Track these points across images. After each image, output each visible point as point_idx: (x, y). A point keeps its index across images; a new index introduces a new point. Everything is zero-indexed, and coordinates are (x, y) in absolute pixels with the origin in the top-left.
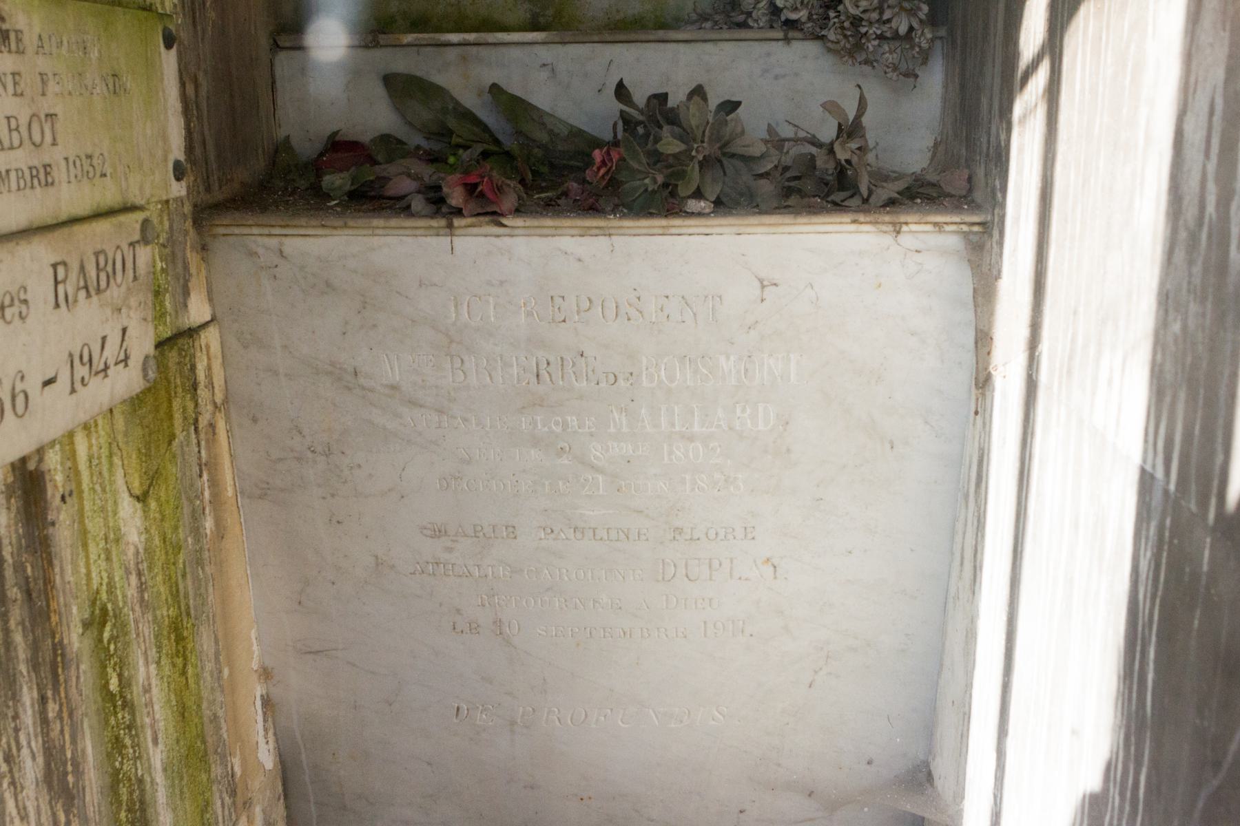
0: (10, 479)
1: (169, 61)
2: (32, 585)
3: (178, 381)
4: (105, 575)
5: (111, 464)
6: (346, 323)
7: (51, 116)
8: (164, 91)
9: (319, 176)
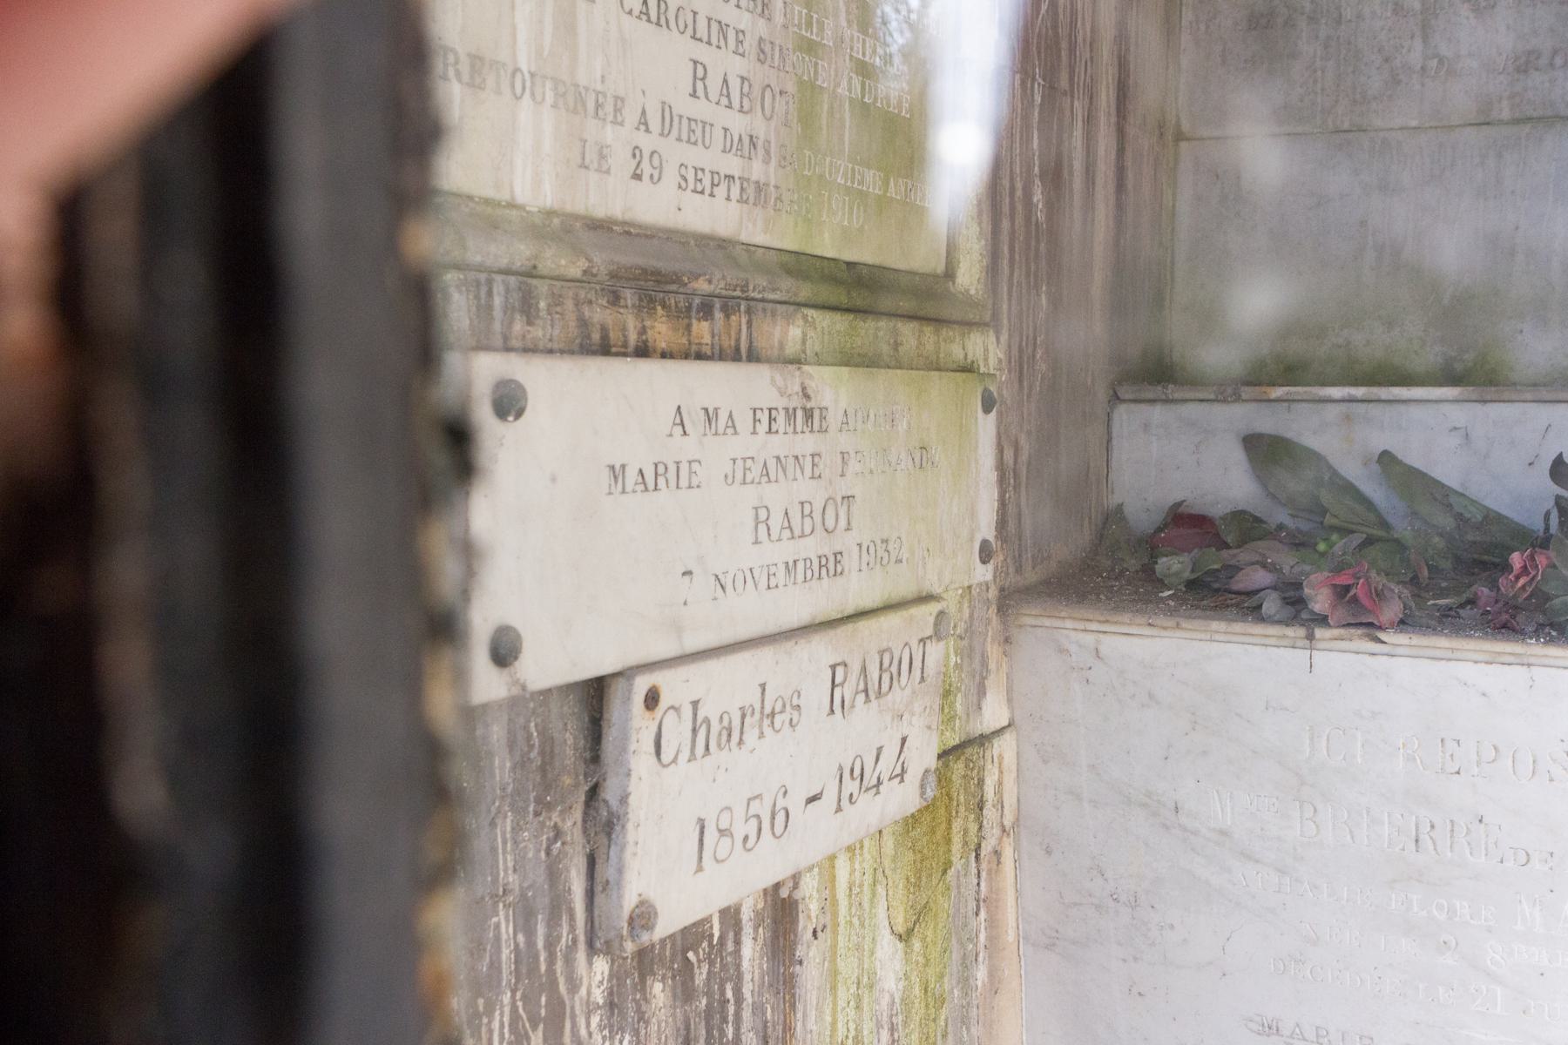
0: (761, 905)
1: (986, 427)
2: (770, 1030)
3: (962, 798)
4: (852, 1026)
5: (874, 894)
6: (1170, 746)
7: (847, 498)
8: (977, 461)
9: (1154, 558)
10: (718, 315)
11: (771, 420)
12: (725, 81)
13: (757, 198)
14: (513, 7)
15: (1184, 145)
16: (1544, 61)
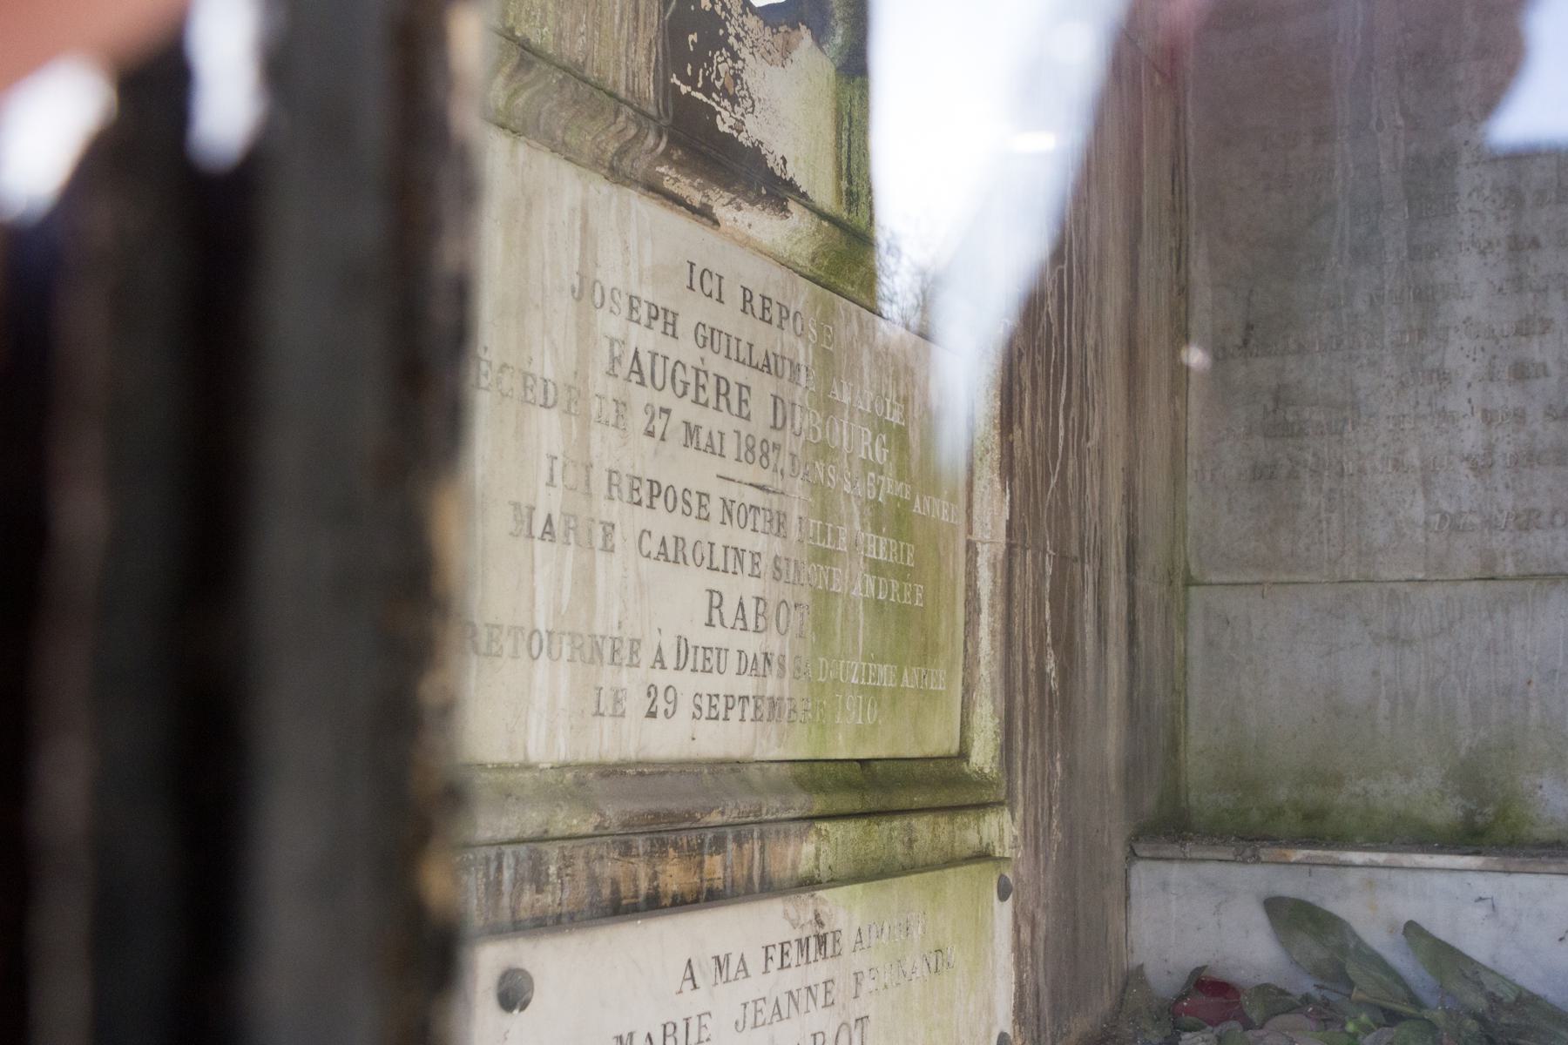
1: (1003, 913)
8: (993, 953)
10: (731, 846)
11: (784, 954)
12: (741, 604)
13: (771, 713)
14: (533, 572)
15: (1193, 589)
16: (1544, 519)
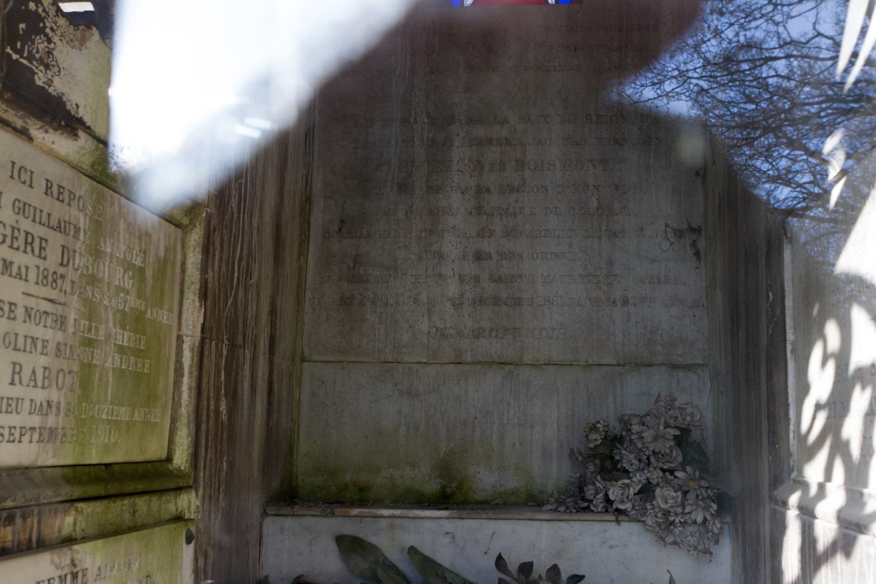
1: (188, 552)
8: (181, 575)
10: (19, 521)
15: (305, 364)
16: (487, 333)
